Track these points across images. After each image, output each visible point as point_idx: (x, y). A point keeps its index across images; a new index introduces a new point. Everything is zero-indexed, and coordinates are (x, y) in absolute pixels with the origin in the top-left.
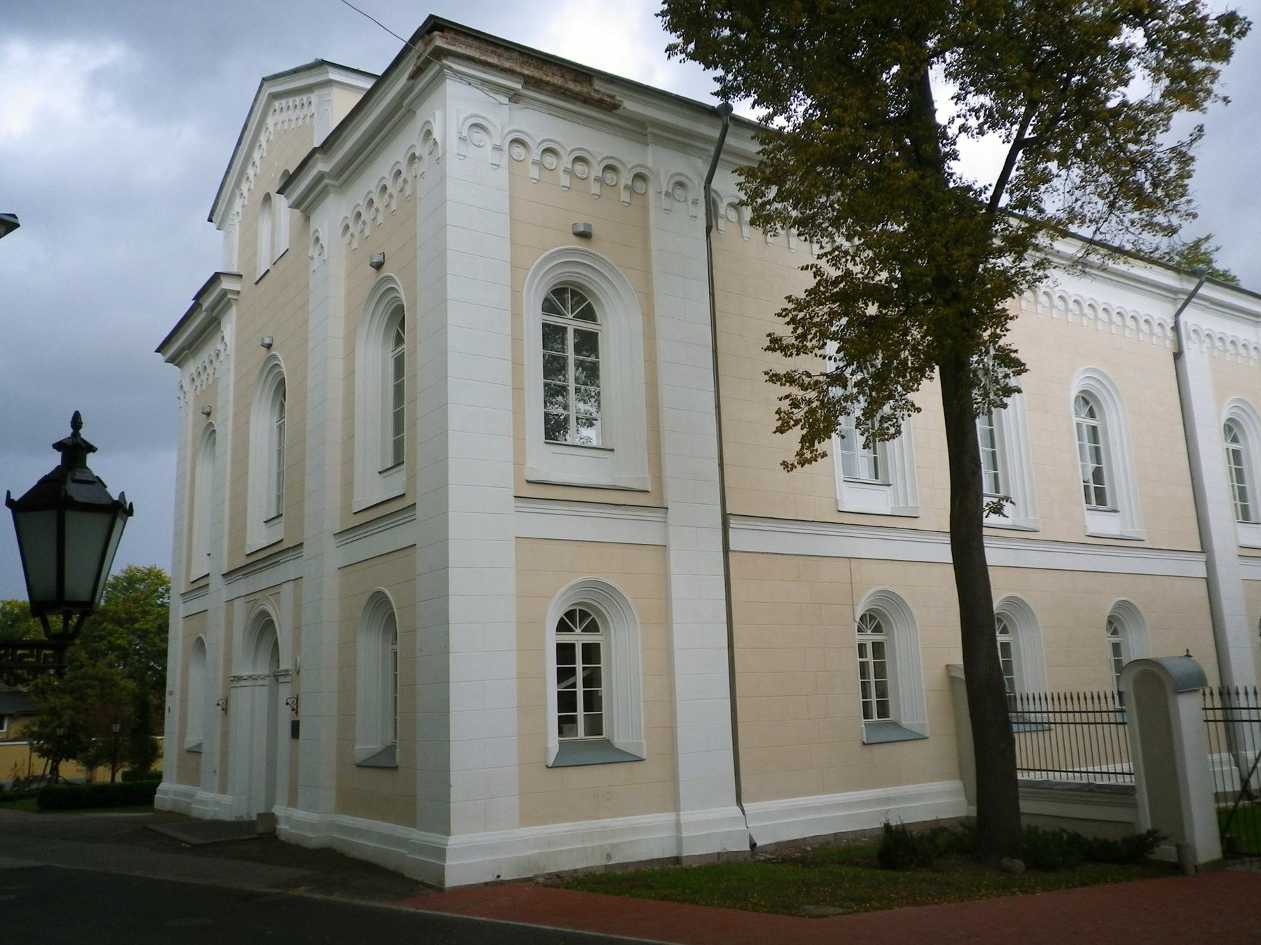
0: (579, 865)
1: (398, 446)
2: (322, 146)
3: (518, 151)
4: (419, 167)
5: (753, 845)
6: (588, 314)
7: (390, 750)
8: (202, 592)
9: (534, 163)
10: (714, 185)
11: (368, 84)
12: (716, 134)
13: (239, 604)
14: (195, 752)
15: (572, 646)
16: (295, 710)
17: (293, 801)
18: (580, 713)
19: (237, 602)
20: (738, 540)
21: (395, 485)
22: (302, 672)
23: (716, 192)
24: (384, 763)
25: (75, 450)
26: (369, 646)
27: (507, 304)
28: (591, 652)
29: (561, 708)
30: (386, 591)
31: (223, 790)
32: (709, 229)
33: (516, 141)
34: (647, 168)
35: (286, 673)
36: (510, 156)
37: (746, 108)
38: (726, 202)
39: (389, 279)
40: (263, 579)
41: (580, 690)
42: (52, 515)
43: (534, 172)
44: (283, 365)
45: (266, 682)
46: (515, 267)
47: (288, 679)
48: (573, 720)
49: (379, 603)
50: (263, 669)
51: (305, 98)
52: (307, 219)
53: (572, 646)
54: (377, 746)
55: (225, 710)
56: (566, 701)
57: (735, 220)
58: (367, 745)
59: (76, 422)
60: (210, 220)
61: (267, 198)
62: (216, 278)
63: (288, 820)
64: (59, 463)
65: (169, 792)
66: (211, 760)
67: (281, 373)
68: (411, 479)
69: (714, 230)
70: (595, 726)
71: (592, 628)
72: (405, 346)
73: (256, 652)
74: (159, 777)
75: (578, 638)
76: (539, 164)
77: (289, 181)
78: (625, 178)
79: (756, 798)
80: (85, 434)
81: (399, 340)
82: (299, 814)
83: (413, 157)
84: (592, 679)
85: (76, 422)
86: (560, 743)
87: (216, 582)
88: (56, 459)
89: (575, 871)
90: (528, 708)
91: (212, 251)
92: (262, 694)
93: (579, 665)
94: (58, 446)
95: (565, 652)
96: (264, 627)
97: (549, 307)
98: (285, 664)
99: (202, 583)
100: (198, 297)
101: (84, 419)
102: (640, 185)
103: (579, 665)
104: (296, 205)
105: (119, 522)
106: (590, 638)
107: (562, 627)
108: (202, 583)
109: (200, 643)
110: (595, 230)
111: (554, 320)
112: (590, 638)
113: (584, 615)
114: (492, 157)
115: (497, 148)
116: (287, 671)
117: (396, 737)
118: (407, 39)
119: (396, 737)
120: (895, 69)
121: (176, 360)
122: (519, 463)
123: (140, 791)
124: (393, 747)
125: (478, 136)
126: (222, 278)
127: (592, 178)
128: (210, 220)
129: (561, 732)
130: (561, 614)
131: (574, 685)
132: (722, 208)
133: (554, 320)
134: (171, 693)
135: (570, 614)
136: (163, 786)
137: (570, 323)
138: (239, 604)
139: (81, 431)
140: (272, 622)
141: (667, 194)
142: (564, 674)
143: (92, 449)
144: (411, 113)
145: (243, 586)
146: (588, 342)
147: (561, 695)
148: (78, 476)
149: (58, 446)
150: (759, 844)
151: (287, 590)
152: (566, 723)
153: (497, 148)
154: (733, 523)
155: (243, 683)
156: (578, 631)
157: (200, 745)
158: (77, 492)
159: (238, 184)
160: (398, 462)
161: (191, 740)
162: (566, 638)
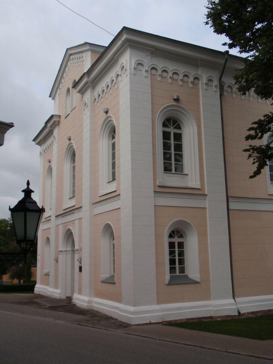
0: (177, 319)
1: (114, 174)
2: (87, 72)
3: (154, 72)
4: (120, 78)
5: (239, 313)
6: (179, 127)
7: (112, 277)
8: (49, 222)
9: (159, 75)
10: (223, 79)
11: (102, 50)
12: (223, 62)
13: (61, 226)
14: (47, 275)
15: (174, 243)
16: (80, 263)
17: (80, 293)
18: (177, 266)
19: (60, 225)
20: (232, 206)
21: (112, 187)
22: (83, 250)
23: (223, 82)
24: (110, 281)
25: (28, 192)
26: (104, 243)
27: (151, 125)
28: (181, 245)
29: (170, 264)
30: (110, 223)
31: (56, 287)
32: (221, 95)
33: (153, 68)
34: (199, 75)
35: (77, 250)
36: (151, 74)
37: (235, 52)
38: (227, 85)
39: (110, 117)
40: (69, 218)
41: (177, 258)
42: (22, 214)
43: (159, 79)
44: (74, 146)
45: (70, 253)
46: (153, 112)
47: (78, 252)
48: (175, 268)
49: (108, 228)
50: (69, 249)
51: (81, 55)
52: (82, 97)
53: (174, 243)
54: (108, 276)
55: (57, 262)
56: (172, 262)
57: (230, 91)
58: (105, 275)
59: (28, 183)
60: (50, 97)
61: (68, 90)
62: (52, 117)
63: (78, 299)
64: (23, 197)
65: (39, 288)
66: (52, 278)
67: (73, 149)
68: (119, 185)
69: (222, 96)
70: (182, 270)
71: (181, 236)
72: (116, 139)
73: (67, 242)
74: (35, 283)
75: (176, 240)
76: (161, 76)
77: (75, 85)
78: (191, 79)
79: (240, 296)
80: (31, 187)
81: (113, 137)
82: (82, 297)
83: (118, 75)
84: (181, 254)
85: (28, 183)
86: (171, 276)
87: (53, 218)
88: (22, 196)
89: (176, 320)
90: (159, 264)
91: (50, 108)
92: (69, 256)
93: (177, 249)
94: (23, 191)
95: (171, 245)
96: (69, 235)
97: (164, 125)
98: (76, 247)
99: (48, 219)
100: (47, 123)
101: (30, 182)
102: (196, 81)
103: (177, 249)
104: (79, 92)
105: (41, 214)
106: (180, 240)
107: (171, 236)
108: (48, 219)
109: (48, 239)
110: (181, 98)
111: (167, 129)
112: (180, 240)
113: (178, 232)
114: (145, 74)
115: (146, 71)
116: (78, 249)
117: (114, 272)
118: (115, 35)
119: (114, 272)
120: (266, 23)
121: (39, 144)
122: (155, 180)
123: (30, 287)
124: (113, 276)
125: (140, 67)
126: (54, 116)
127: (179, 79)
128: (50, 97)
129: (171, 272)
130: (170, 232)
131: (175, 256)
132: (225, 88)
133: (167, 129)
134: (39, 255)
135: (173, 232)
136: (37, 286)
137: (172, 130)
138: (61, 226)
139: (29, 186)
140: (72, 233)
141: (206, 84)
142: (172, 253)
143: (33, 192)
144: (117, 61)
145: (61, 220)
146: (178, 137)
147: (170, 260)
148: (30, 201)
149: (23, 191)
150: (242, 312)
151: (77, 222)
152: (172, 269)
153: (146, 71)
154: (230, 200)
155: (62, 253)
156: (176, 237)
157: (49, 272)
158: (29, 206)
159: (59, 85)
160: (114, 179)
161: (46, 271)
162: (172, 240)
